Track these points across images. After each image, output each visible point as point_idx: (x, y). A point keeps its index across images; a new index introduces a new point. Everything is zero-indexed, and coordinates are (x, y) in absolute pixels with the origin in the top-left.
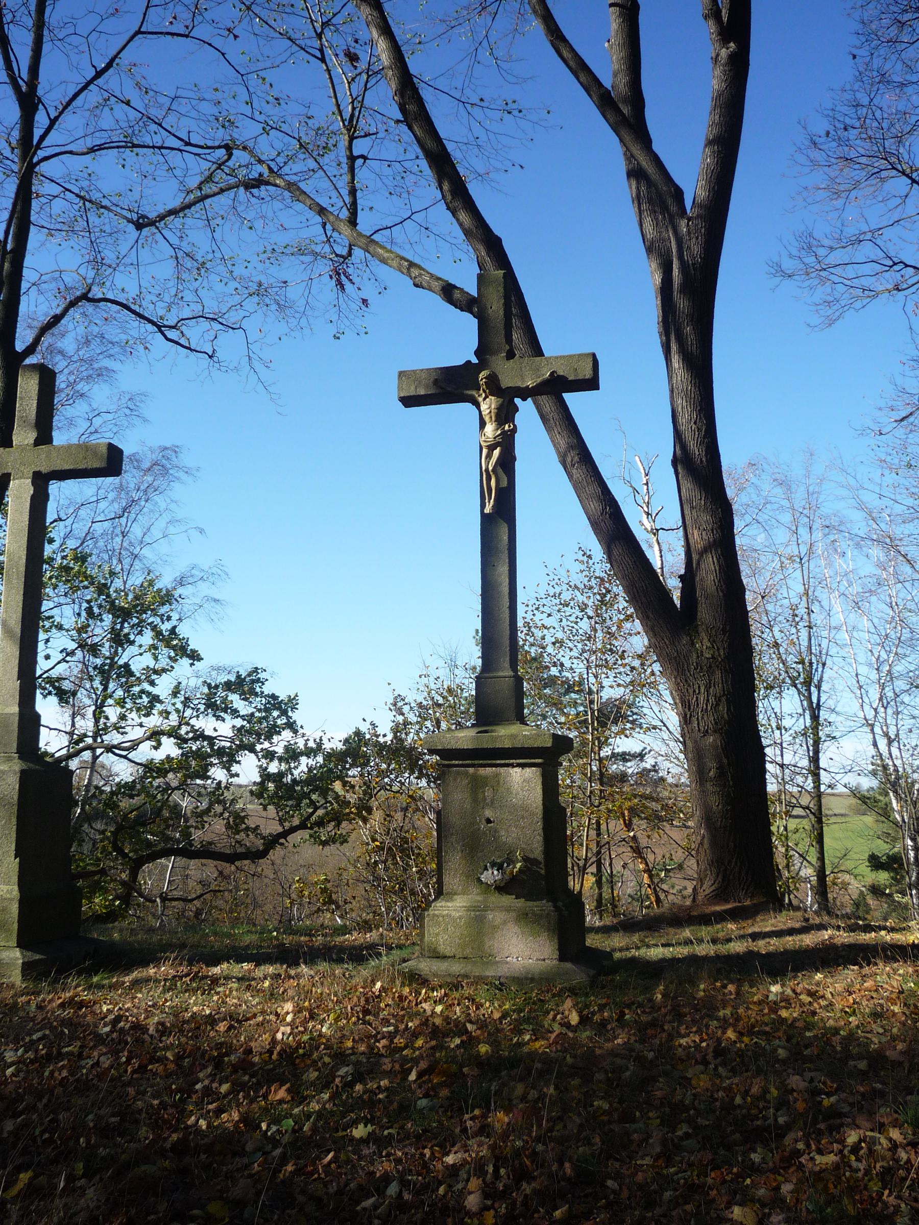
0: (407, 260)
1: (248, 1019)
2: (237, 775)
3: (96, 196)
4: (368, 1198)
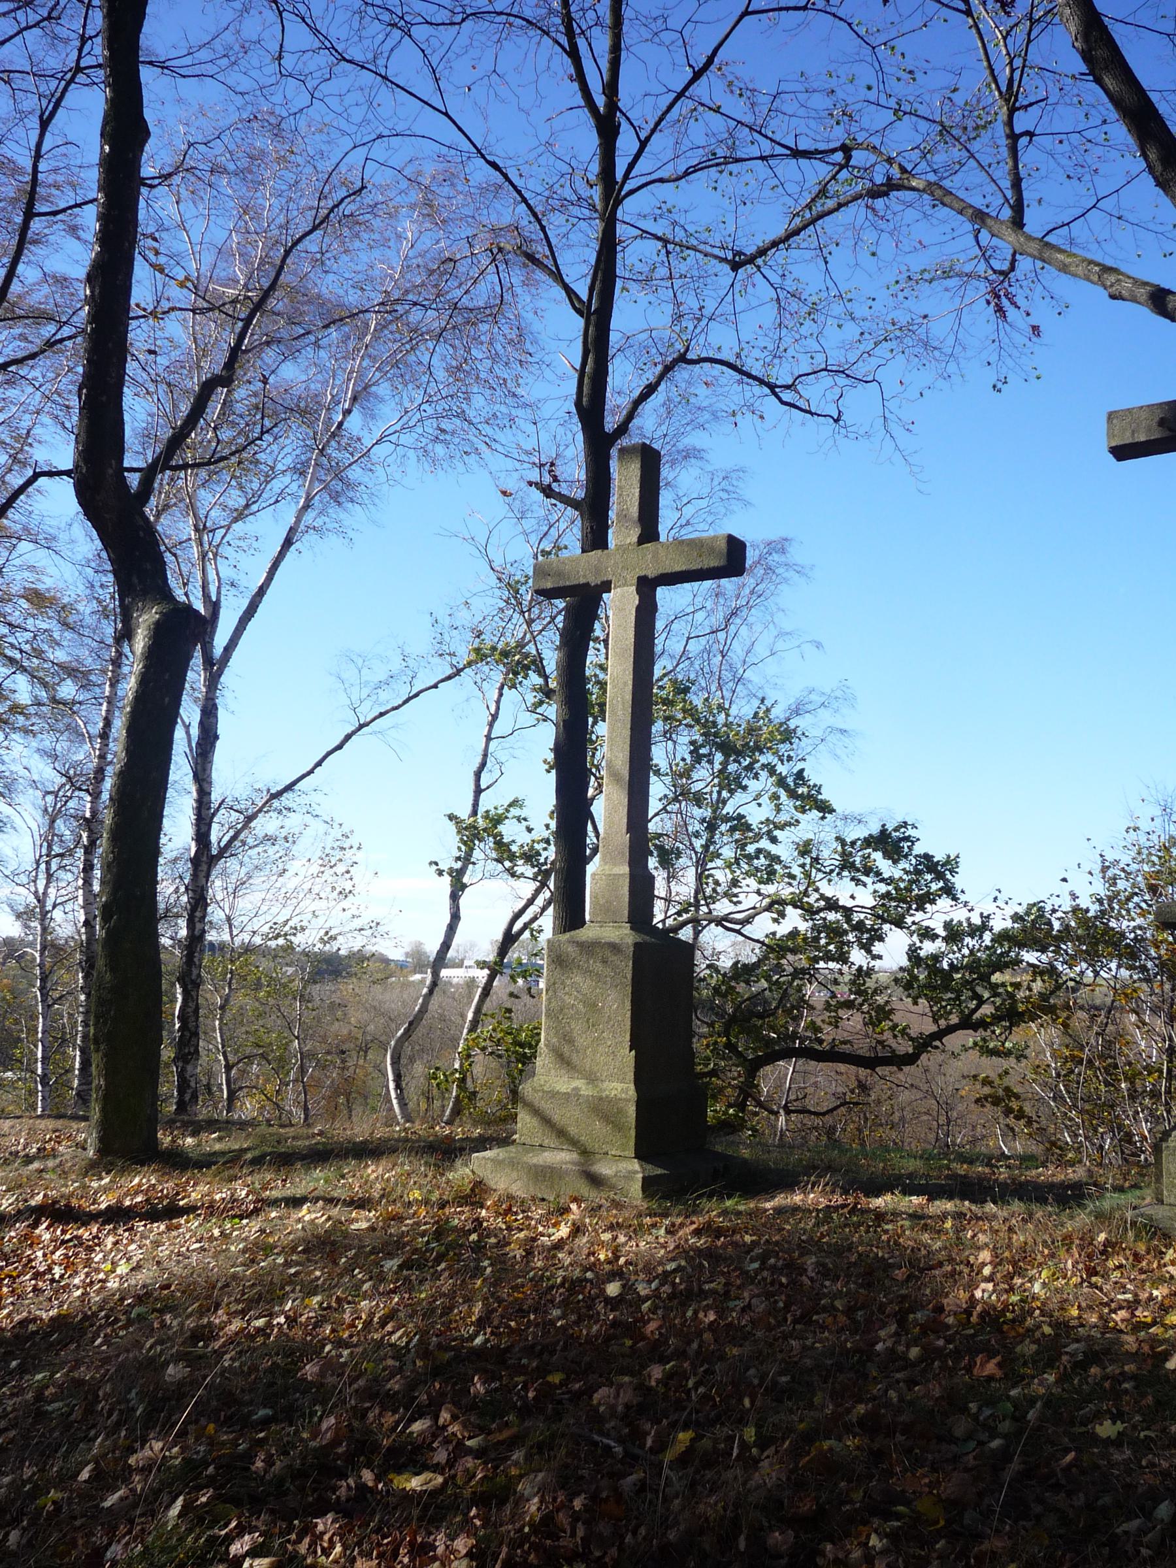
0: (1098, 264)
1: (931, 1268)
2: (880, 957)
3: (680, 235)
4: (1129, 1519)
